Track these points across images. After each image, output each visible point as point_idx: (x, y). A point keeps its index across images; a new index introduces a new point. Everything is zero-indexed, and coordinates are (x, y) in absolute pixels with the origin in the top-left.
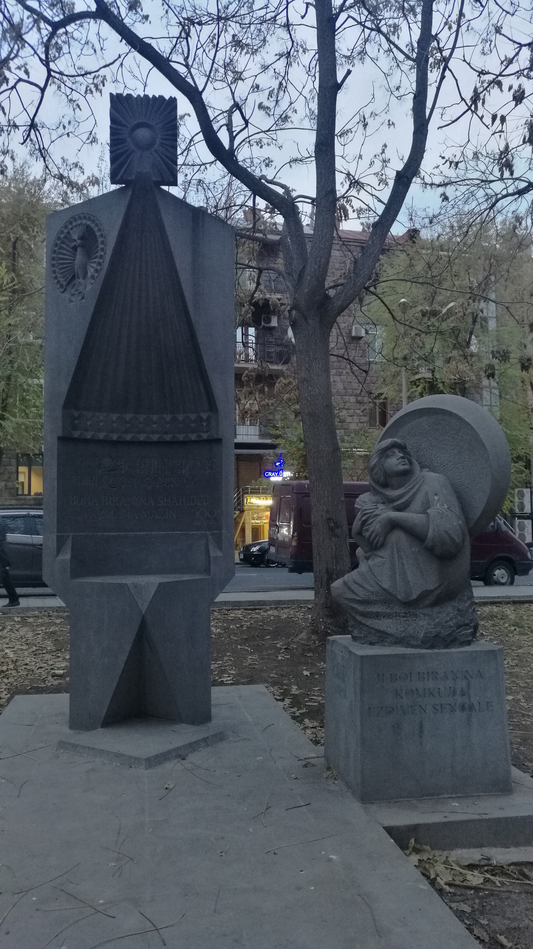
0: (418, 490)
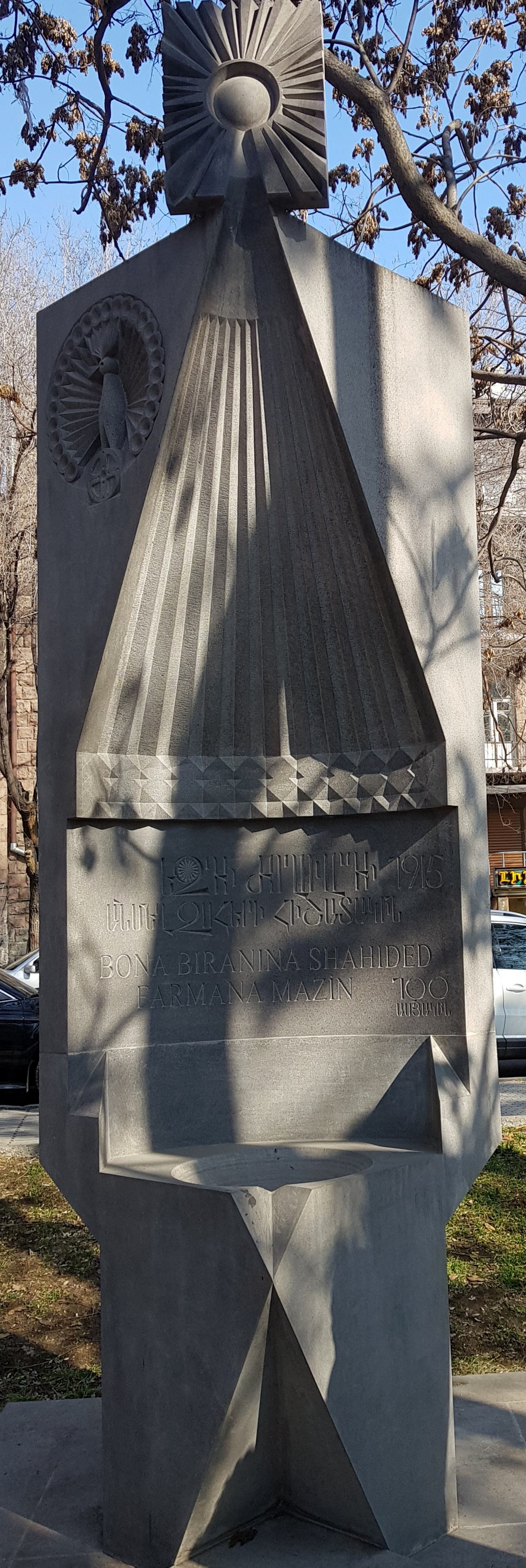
0: (194, 92)
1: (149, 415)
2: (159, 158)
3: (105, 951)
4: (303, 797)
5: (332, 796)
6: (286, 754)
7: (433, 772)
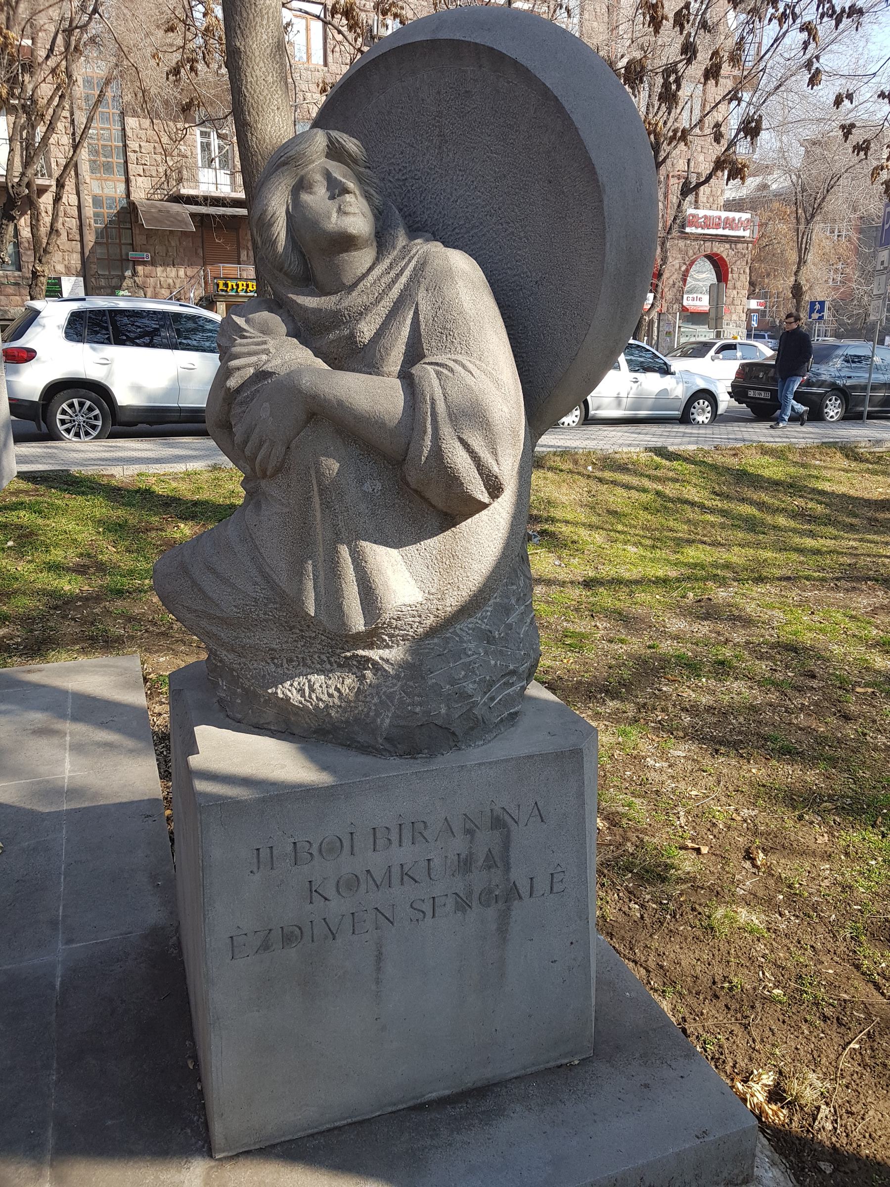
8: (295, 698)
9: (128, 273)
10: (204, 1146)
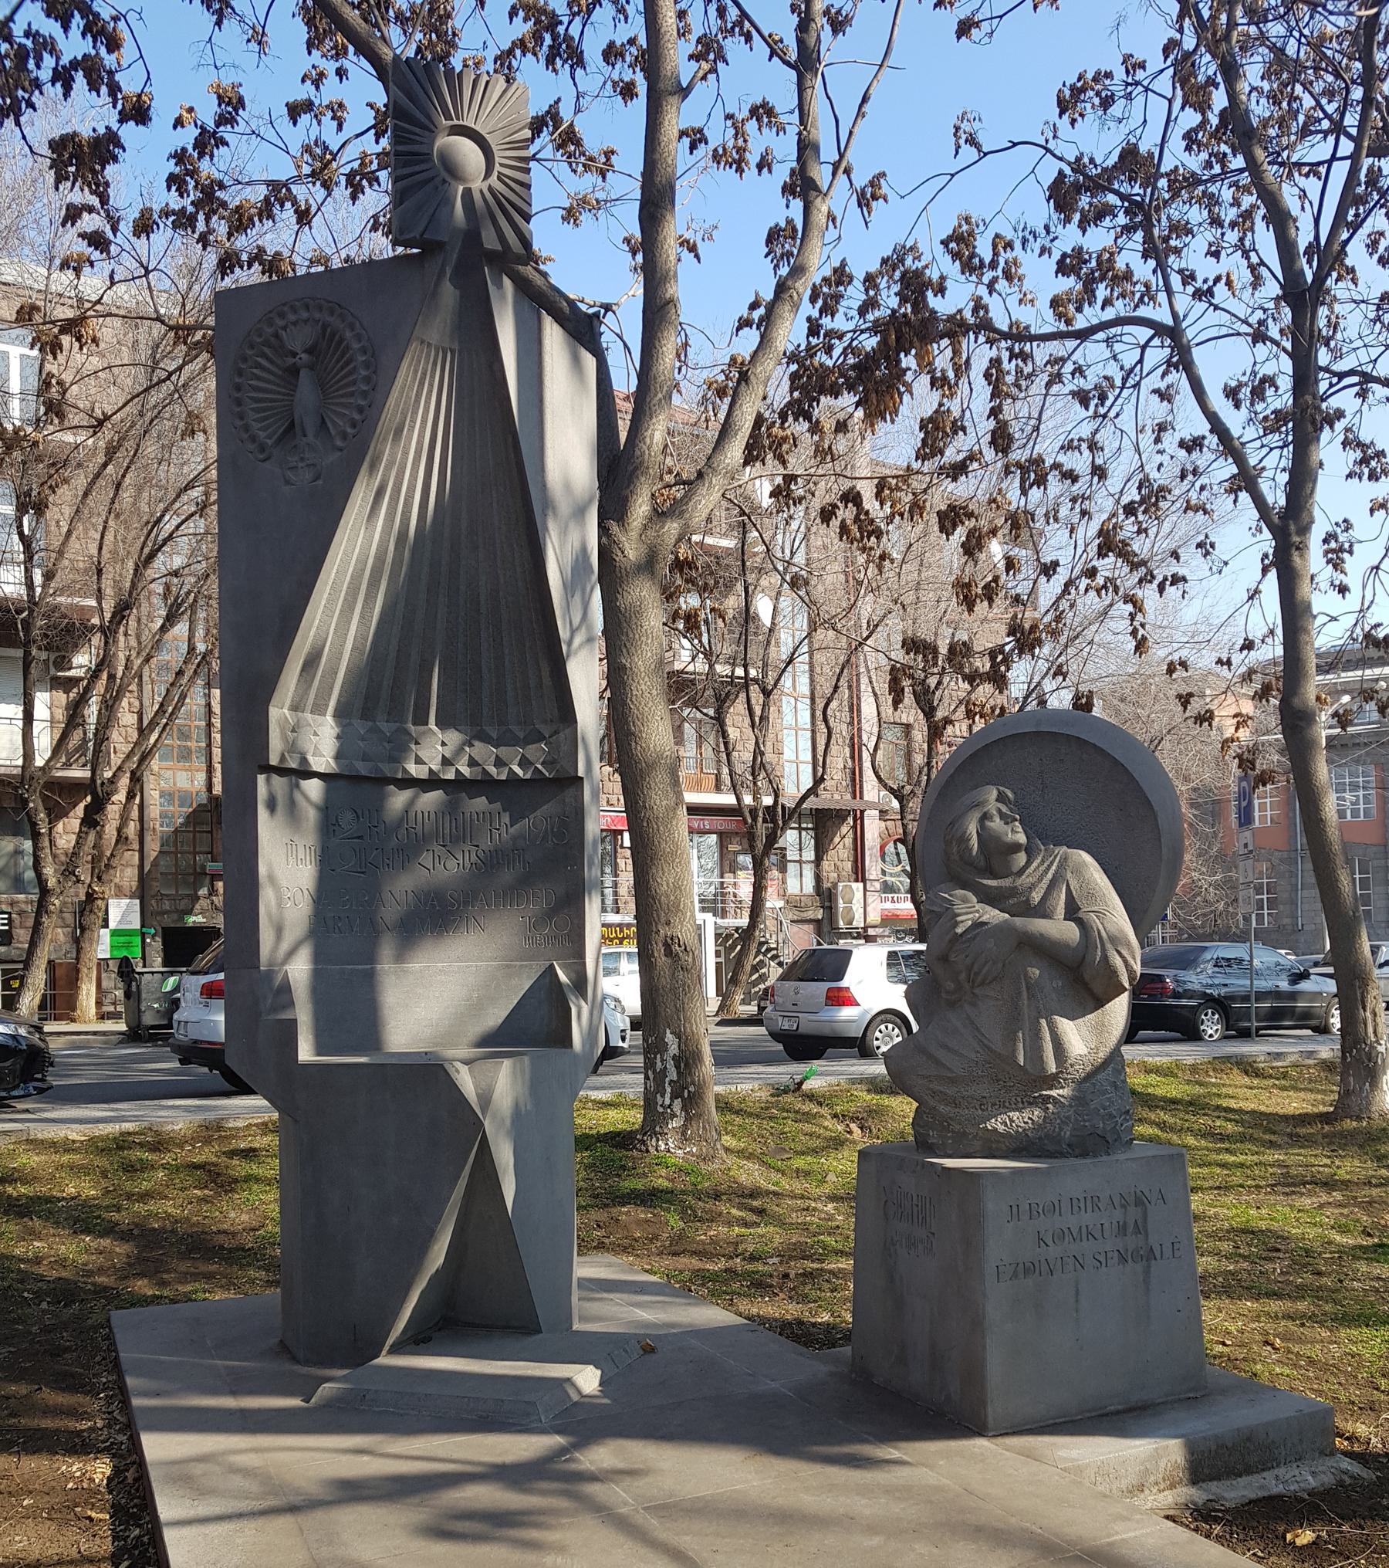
1: (357, 417)
2: (84, 35)
3: (284, 883)
4: (446, 762)
5: (472, 763)
6: (432, 726)
7: (564, 748)
8: (1001, 1128)
9: (203, 892)
10: (977, 1429)
